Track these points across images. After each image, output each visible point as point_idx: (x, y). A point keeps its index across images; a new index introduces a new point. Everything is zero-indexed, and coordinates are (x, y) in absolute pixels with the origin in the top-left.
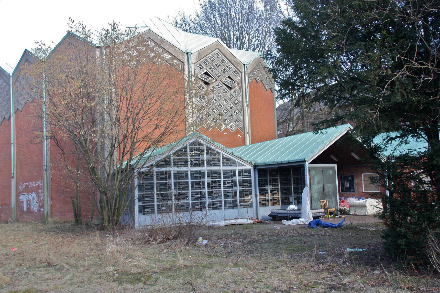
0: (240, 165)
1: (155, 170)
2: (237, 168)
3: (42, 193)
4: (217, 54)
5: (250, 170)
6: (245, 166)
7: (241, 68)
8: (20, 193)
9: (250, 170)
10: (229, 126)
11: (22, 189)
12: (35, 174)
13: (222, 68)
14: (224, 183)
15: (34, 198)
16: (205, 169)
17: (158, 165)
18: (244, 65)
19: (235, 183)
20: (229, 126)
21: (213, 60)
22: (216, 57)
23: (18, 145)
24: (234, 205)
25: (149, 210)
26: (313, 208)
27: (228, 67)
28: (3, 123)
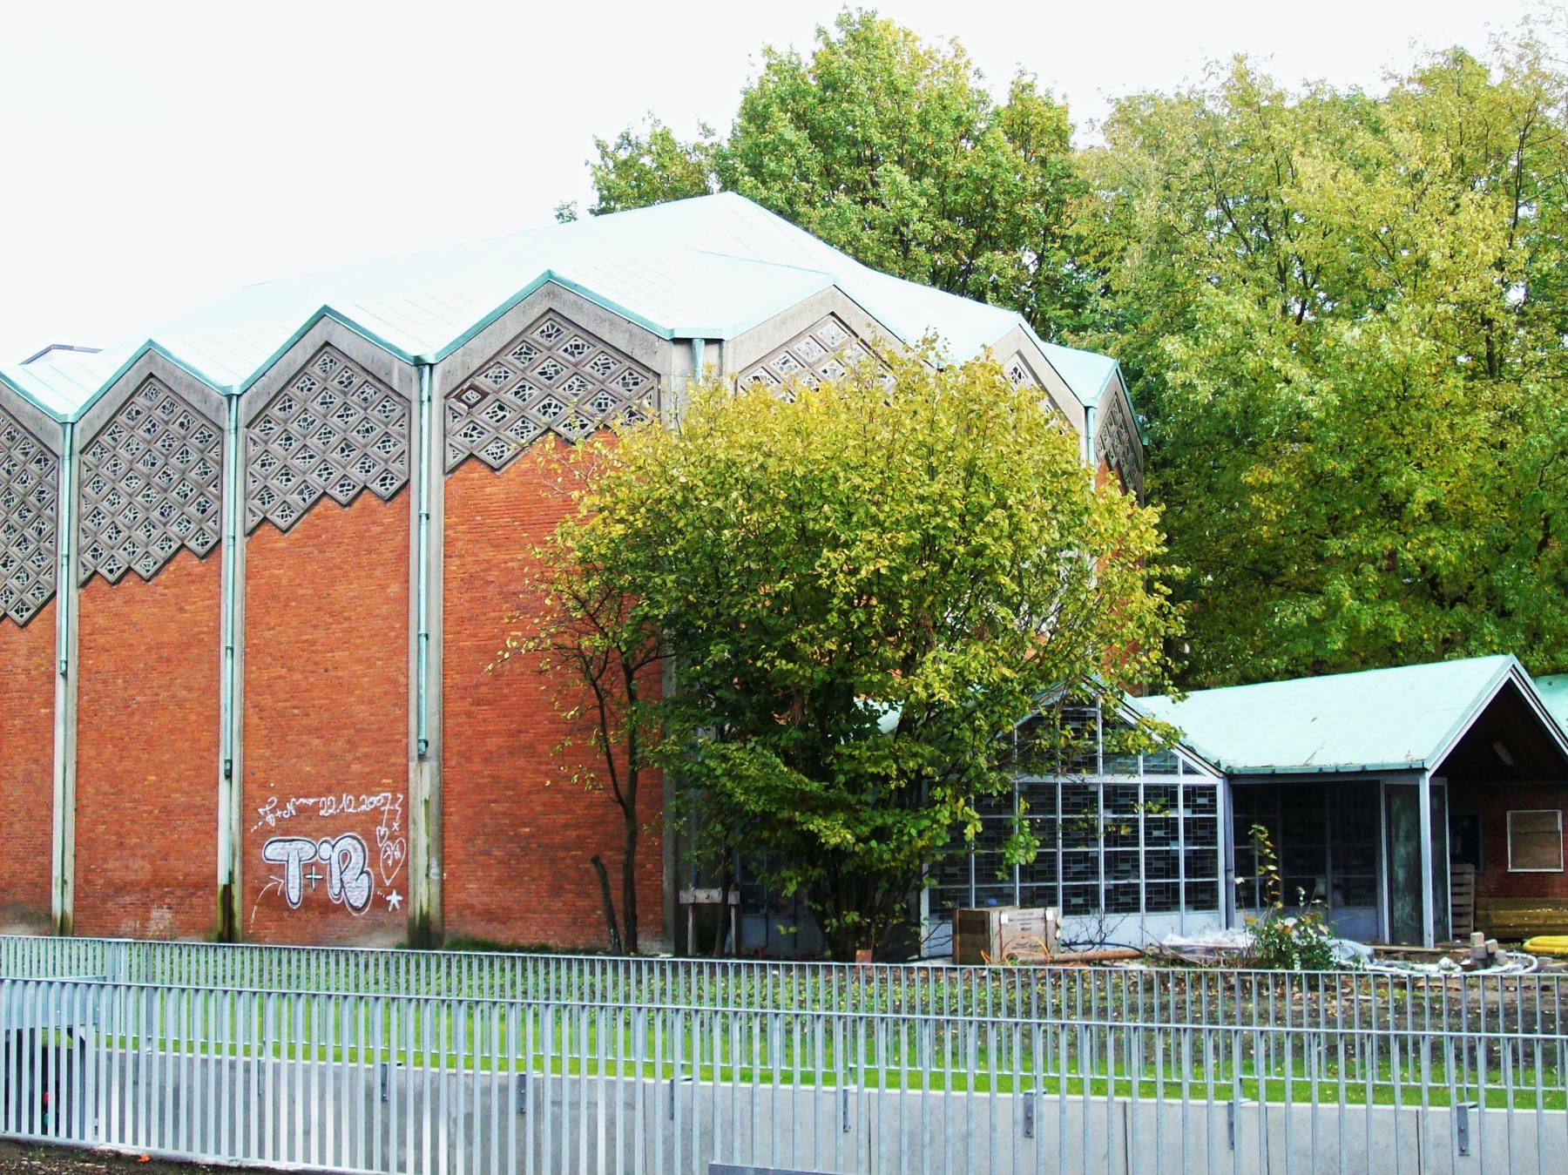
0: (1189, 771)
2: (1182, 780)
3: (392, 838)
5: (1213, 788)
8: (266, 832)
9: (1213, 788)
11: (278, 820)
12: (356, 767)
15: (345, 856)
18: (1087, 409)
23: (252, 653)
26: (743, 951)
28: (171, 567)
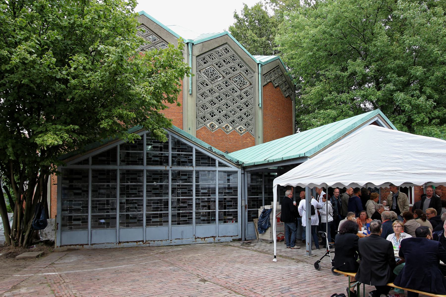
0: (221, 165)
1: (90, 167)
4: (226, 49)
6: (229, 167)
7: (255, 68)
10: (237, 128)
13: (232, 64)
14: (196, 193)
16: (170, 168)
17: (96, 160)
19: (167, 203)
20: (237, 128)
21: (220, 56)
22: (225, 53)
24: (209, 219)
25: (80, 222)
27: (239, 65)
